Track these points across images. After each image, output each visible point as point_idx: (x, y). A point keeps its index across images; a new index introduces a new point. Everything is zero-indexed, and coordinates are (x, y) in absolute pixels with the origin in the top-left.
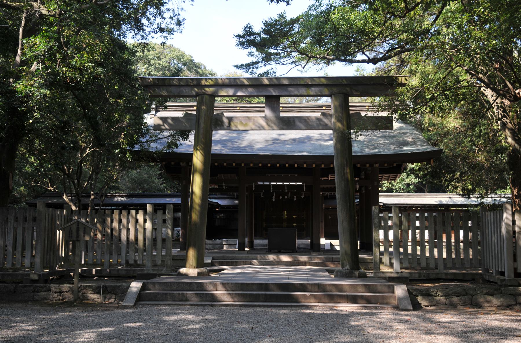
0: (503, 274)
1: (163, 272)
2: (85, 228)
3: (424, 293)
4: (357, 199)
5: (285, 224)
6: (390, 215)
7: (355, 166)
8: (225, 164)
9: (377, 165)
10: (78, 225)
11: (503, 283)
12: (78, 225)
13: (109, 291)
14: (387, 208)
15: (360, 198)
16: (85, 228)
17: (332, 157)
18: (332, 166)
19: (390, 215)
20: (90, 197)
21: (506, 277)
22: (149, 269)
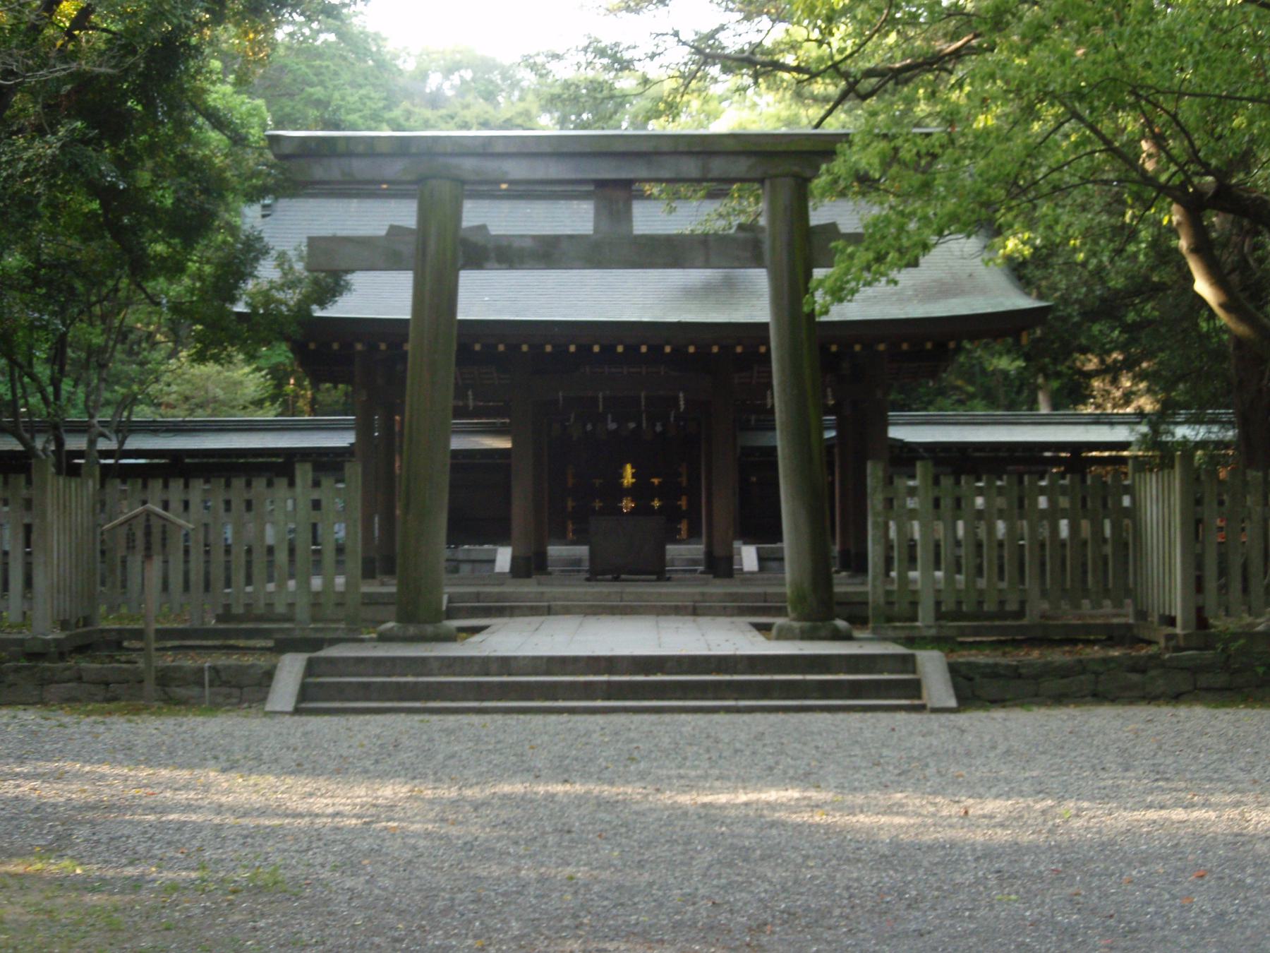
0: (1171, 621)
1: (341, 634)
2: (164, 526)
3: (988, 670)
4: (829, 428)
5: (627, 504)
6: (911, 483)
7: (824, 349)
8: (477, 347)
9: (882, 347)
10: (148, 520)
11: (1172, 643)
12: (148, 520)
13: (224, 678)
14: (907, 455)
15: (839, 427)
16: (164, 526)
17: (764, 327)
18: (763, 349)
19: (911, 483)
20: (749, 538)
21: (1178, 630)
22: (304, 627)
